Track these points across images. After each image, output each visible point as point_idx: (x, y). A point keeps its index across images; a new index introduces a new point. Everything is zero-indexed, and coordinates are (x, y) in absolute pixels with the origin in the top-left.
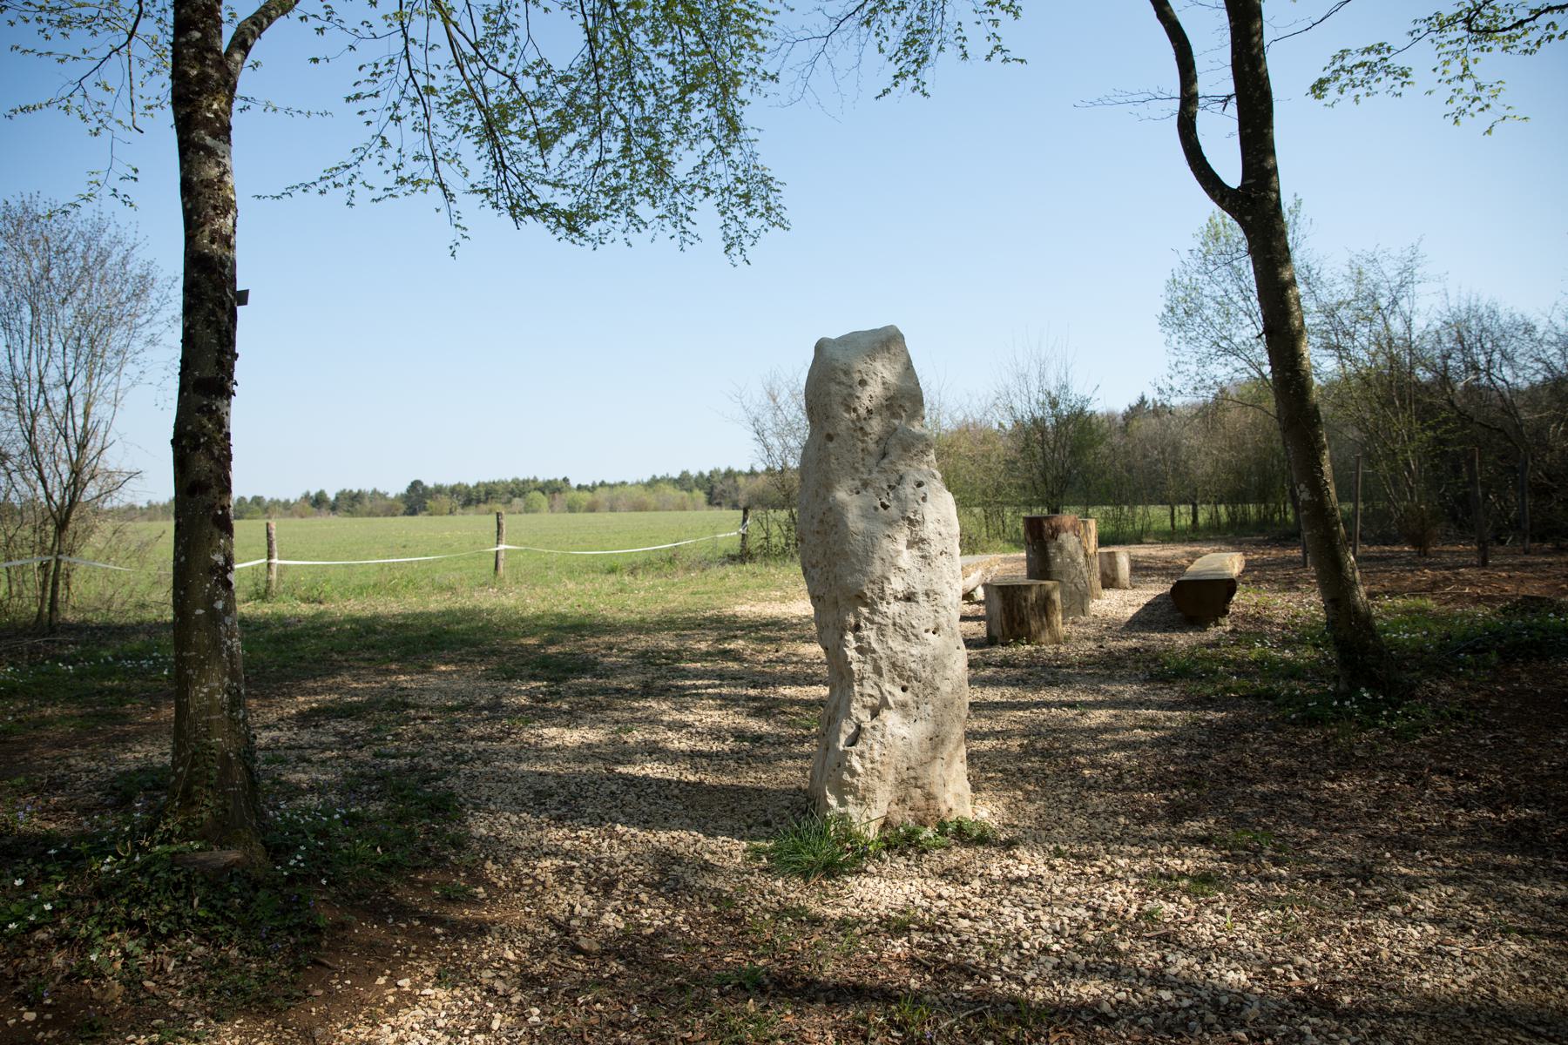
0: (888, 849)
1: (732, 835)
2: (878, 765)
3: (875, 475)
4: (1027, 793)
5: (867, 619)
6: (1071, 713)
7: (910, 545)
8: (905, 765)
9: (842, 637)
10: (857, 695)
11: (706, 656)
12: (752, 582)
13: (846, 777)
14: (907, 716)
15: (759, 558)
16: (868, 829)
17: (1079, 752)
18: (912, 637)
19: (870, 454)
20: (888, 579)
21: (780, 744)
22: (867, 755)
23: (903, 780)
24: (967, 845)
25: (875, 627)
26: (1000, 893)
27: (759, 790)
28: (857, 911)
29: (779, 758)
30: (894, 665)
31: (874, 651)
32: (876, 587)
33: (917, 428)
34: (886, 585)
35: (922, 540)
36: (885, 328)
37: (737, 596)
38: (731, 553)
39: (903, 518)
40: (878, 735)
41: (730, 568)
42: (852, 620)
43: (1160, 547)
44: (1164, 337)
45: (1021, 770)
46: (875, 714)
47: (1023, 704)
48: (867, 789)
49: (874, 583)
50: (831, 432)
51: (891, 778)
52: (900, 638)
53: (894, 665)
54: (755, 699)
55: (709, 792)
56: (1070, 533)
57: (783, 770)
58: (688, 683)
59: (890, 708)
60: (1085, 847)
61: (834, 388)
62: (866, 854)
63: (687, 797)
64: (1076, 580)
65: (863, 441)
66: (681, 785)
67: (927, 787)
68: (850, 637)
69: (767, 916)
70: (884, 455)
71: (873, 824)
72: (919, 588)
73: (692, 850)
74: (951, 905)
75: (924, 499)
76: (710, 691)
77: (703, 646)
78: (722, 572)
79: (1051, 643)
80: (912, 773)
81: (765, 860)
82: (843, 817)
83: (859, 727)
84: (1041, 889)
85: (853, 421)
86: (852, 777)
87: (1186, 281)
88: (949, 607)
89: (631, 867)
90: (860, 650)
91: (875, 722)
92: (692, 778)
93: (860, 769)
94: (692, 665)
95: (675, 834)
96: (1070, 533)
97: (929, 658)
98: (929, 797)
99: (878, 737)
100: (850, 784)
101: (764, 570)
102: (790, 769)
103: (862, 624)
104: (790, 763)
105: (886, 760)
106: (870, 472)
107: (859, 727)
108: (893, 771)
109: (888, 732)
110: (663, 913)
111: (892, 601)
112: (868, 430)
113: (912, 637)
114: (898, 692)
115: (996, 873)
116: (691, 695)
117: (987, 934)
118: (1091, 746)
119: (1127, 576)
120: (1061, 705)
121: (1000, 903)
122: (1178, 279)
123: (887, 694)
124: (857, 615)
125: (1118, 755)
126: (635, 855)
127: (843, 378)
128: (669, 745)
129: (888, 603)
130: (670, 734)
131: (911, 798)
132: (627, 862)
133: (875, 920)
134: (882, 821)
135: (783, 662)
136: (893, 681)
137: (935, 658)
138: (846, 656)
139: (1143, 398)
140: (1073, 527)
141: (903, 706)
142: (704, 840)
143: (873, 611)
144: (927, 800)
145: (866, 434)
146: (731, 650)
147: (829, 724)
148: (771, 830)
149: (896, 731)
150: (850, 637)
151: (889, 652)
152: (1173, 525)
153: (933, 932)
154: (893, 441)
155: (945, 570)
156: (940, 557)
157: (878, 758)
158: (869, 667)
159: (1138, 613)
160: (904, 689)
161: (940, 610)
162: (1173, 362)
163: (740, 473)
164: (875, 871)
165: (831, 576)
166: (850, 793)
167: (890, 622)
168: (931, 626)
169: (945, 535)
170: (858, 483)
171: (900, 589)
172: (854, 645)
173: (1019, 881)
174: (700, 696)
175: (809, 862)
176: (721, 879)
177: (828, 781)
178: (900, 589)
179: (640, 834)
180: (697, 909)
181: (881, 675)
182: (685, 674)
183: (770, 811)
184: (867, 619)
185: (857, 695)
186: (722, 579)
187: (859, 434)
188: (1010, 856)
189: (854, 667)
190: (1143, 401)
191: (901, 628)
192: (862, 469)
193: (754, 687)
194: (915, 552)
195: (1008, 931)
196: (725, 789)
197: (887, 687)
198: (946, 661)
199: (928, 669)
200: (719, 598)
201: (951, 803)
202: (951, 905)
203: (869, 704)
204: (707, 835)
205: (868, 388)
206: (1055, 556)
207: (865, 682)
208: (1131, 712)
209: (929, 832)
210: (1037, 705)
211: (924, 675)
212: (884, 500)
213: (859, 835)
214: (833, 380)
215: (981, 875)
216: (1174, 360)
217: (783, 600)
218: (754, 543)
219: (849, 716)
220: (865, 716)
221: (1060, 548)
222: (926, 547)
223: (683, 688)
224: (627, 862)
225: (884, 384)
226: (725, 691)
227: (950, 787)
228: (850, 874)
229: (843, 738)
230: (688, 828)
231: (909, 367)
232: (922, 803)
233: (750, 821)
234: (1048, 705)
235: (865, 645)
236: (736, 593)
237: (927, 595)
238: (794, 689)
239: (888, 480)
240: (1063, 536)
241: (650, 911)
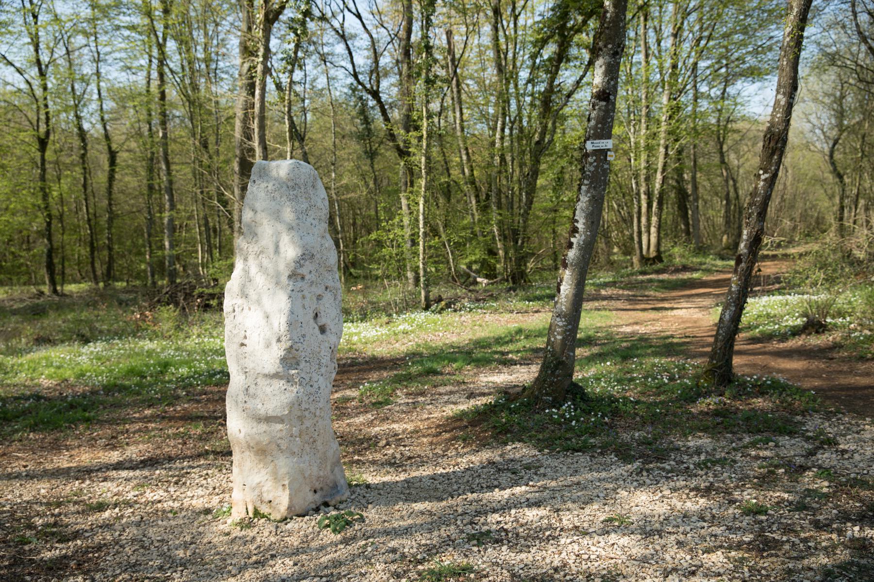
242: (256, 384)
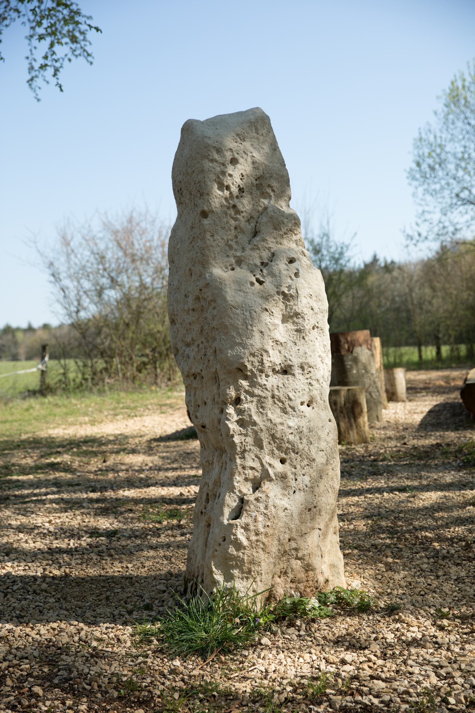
0: (276, 621)
1: (114, 621)
2: (262, 538)
3: (248, 252)
4: (387, 564)
5: (247, 392)
6: (403, 496)
7: (285, 319)
8: (287, 536)
9: (222, 411)
10: (239, 468)
11: (36, 469)
12: (57, 411)
13: (232, 550)
14: (286, 487)
15: (59, 392)
16: (254, 603)
17: (422, 528)
18: (289, 409)
19: (242, 231)
20: (266, 351)
21: (136, 537)
22: (252, 528)
23: (285, 552)
24: (350, 614)
25: (255, 399)
26: (401, 654)
27: (130, 578)
28: (266, 682)
29: (140, 548)
30: (273, 437)
31: (255, 424)
32: (255, 360)
33: (282, 206)
34: (265, 358)
35: (297, 315)
36: (251, 110)
37: (47, 422)
38: (31, 388)
39: (278, 293)
40: (262, 506)
41: (32, 401)
42: (232, 393)
43: (415, 373)
44: (412, 189)
45: (375, 546)
46: (256, 487)
47: (354, 491)
48: (252, 562)
49: (253, 355)
50: (206, 208)
51: (274, 549)
52: (278, 411)
53: (273, 437)
54: (98, 501)
55: (78, 584)
56: (364, 347)
57: (148, 558)
58: (26, 492)
59: (271, 480)
60: (463, 609)
61: (207, 164)
62: (257, 627)
63: (55, 590)
64: (371, 389)
65: (236, 219)
66: (48, 580)
67: (306, 558)
68: (231, 410)
69: (176, 696)
70: (255, 233)
71: (259, 597)
72: (296, 361)
73: (76, 639)
74: (358, 669)
75: (297, 275)
76: (50, 497)
77: (29, 461)
78: (25, 404)
79: (360, 443)
80: (293, 545)
81: (155, 642)
82: (230, 592)
83: (242, 500)
84: (440, 648)
85: (226, 199)
86: (238, 550)
87: (431, 138)
88: (321, 380)
89: (15, 662)
90: (241, 423)
91: (258, 494)
92: (57, 572)
93: (245, 542)
94: (21, 478)
95: (55, 625)
96: (364, 347)
97: (305, 430)
98: (308, 568)
99: (262, 506)
100: (236, 558)
101: (66, 402)
102: (154, 558)
103: (242, 397)
104: (152, 553)
105: (270, 531)
106: (243, 249)
107: (242, 500)
108: (276, 542)
109: (271, 503)
110: (64, 704)
111: (270, 373)
112: (240, 207)
113: (289, 409)
114: (279, 467)
115: (390, 637)
116: (32, 501)
117: (407, 693)
118: (430, 522)
119: (404, 390)
120: (392, 490)
121: (405, 662)
122: (424, 136)
123: (267, 466)
124: (238, 388)
125: (460, 530)
126: (17, 649)
127: (216, 156)
128: (25, 545)
129: (267, 376)
130: (21, 535)
131: (292, 570)
132: (10, 657)
133: (289, 689)
134: (266, 594)
135: (113, 470)
136: (272, 453)
137: (310, 430)
138: (229, 429)
139: (375, 256)
140: (366, 341)
141: (283, 477)
142: (86, 628)
143: (253, 384)
144: (307, 571)
145: (238, 212)
146: (58, 464)
147: (207, 501)
148: (153, 613)
149: (278, 502)
150: (231, 410)
151: (269, 424)
152: (420, 356)
153: (352, 694)
154: (264, 219)
155: (317, 344)
156: (312, 331)
157: (262, 530)
158: (250, 440)
159: (425, 418)
160: (283, 461)
161: (314, 383)
162: (420, 211)
163: (18, 329)
164: (269, 643)
165: (210, 352)
166: (236, 567)
167: (269, 394)
168: (306, 399)
169: (316, 310)
170: (233, 261)
171: (278, 362)
172: (236, 418)
173: (415, 642)
174: (43, 502)
175: (202, 639)
176: (115, 664)
177: (214, 557)
178: (278, 362)
179: (18, 630)
180: (99, 695)
181: (261, 447)
182: (21, 485)
183: (147, 595)
184: (247, 392)
185: (239, 468)
186: (27, 410)
187: (232, 212)
188: (396, 621)
189: (237, 439)
190: (375, 260)
191: (280, 400)
192: (235, 246)
193: (93, 491)
194: (290, 326)
195: (426, 688)
196: (93, 580)
197: (267, 459)
198: (320, 433)
199: (304, 441)
200: (31, 424)
201: (327, 574)
202: (358, 669)
203: (251, 477)
204: (89, 624)
205: (239, 166)
206: (352, 368)
207: (246, 455)
208: (457, 493)
209: (314, 602)
210: (369, 491)
211: (301, 447)
212: (258, 276)
213: (247, 611)
214: (207, 157)
215: (376, 639)
216: (420, 209)
217: (93, 423)
218: (52, 380)
219: (232, 489)
220: (247, 489)
221: (356, 360)
222: (300, 320)
223: (22, 497)
224: (10, 657)
225: (253, 163)
226: (65, 496)
227: (326, 559)
228: (245, 648)
229: (227, 512)
230: (66, 618)
231: (274, 147)
232: (302, 575)
233: (130, 607)
234: (379, 490)
235: (246, 418)
236: (45, 419)
237: (302, 368)
238: (133, 491)
239: (261, 257)
240: (357, 350)
241: (48, 703)
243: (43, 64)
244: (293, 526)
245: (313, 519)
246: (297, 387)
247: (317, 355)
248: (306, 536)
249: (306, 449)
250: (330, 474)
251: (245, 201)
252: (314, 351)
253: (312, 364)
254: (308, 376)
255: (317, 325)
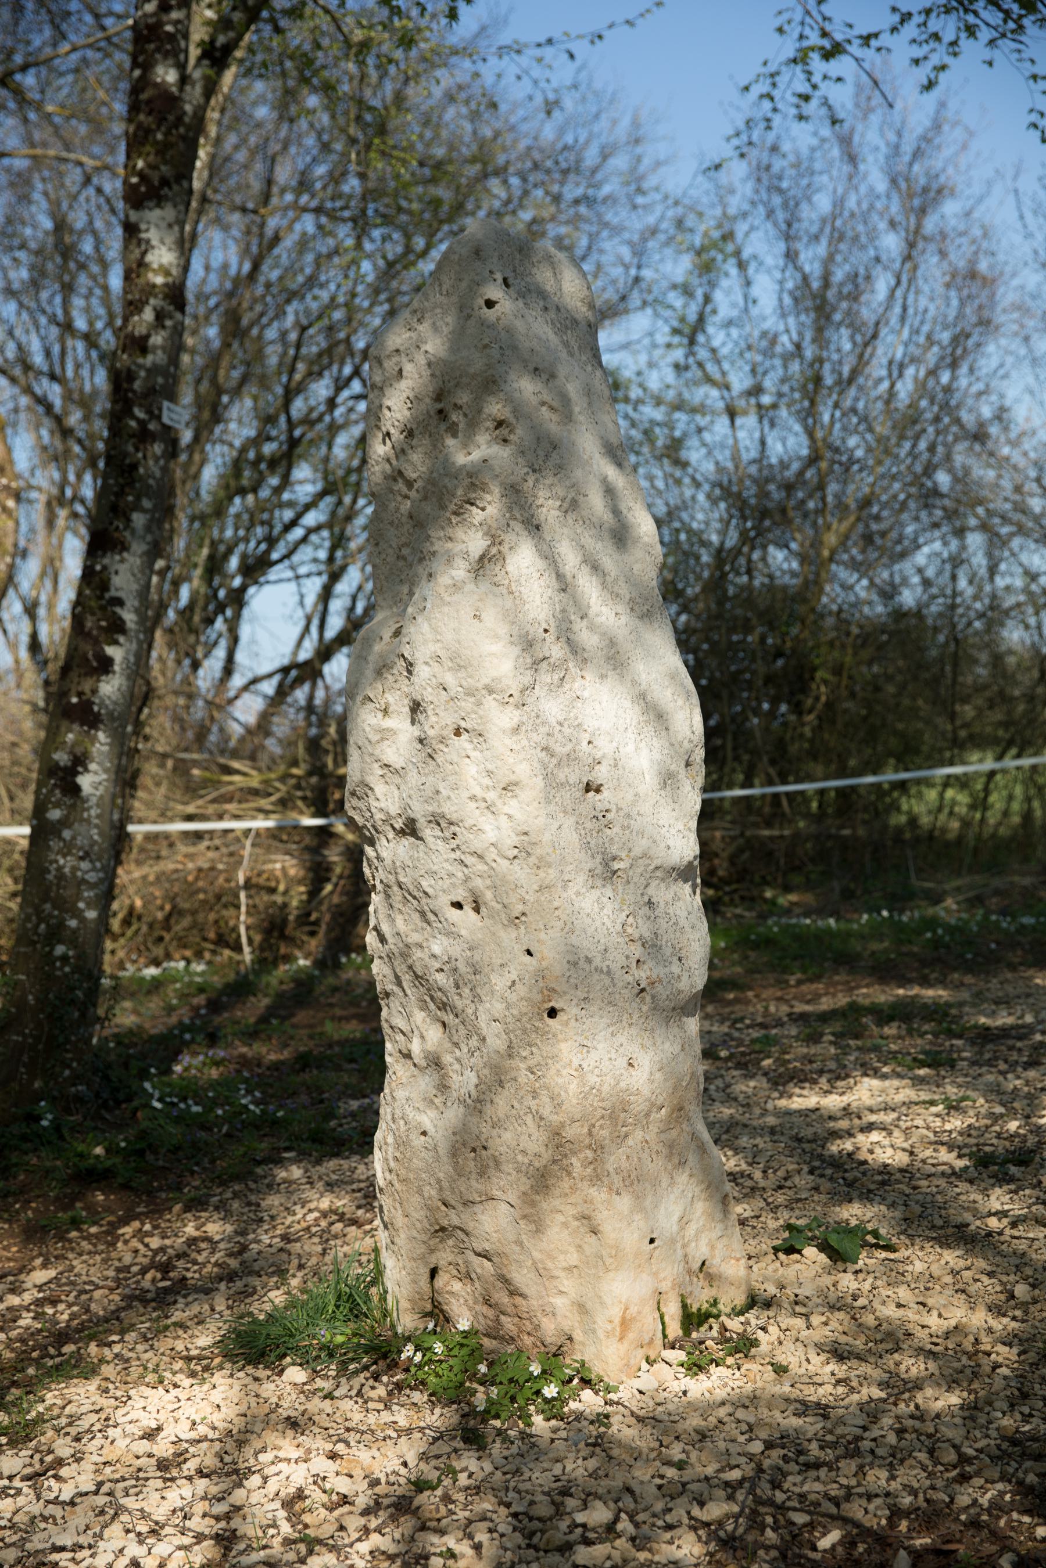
149: (411, 1114)
161: (469, 860)
242: (650, 903)
243: (699, 208)
244: (441, 1175)
245: (482, 1173)
246: (435, 868)
247: (466, 794)
248: (478, 1208)
249: (470, 1011)
250: (522, 1080)
251: (416, 457)
252: (455, 787)
253: (454, 817)
254: (454, 843)
255: (463, 724)
